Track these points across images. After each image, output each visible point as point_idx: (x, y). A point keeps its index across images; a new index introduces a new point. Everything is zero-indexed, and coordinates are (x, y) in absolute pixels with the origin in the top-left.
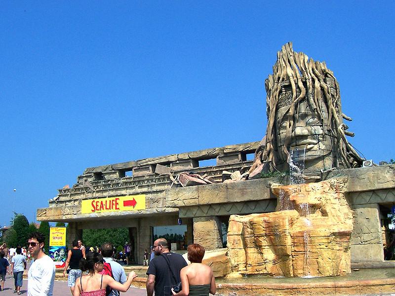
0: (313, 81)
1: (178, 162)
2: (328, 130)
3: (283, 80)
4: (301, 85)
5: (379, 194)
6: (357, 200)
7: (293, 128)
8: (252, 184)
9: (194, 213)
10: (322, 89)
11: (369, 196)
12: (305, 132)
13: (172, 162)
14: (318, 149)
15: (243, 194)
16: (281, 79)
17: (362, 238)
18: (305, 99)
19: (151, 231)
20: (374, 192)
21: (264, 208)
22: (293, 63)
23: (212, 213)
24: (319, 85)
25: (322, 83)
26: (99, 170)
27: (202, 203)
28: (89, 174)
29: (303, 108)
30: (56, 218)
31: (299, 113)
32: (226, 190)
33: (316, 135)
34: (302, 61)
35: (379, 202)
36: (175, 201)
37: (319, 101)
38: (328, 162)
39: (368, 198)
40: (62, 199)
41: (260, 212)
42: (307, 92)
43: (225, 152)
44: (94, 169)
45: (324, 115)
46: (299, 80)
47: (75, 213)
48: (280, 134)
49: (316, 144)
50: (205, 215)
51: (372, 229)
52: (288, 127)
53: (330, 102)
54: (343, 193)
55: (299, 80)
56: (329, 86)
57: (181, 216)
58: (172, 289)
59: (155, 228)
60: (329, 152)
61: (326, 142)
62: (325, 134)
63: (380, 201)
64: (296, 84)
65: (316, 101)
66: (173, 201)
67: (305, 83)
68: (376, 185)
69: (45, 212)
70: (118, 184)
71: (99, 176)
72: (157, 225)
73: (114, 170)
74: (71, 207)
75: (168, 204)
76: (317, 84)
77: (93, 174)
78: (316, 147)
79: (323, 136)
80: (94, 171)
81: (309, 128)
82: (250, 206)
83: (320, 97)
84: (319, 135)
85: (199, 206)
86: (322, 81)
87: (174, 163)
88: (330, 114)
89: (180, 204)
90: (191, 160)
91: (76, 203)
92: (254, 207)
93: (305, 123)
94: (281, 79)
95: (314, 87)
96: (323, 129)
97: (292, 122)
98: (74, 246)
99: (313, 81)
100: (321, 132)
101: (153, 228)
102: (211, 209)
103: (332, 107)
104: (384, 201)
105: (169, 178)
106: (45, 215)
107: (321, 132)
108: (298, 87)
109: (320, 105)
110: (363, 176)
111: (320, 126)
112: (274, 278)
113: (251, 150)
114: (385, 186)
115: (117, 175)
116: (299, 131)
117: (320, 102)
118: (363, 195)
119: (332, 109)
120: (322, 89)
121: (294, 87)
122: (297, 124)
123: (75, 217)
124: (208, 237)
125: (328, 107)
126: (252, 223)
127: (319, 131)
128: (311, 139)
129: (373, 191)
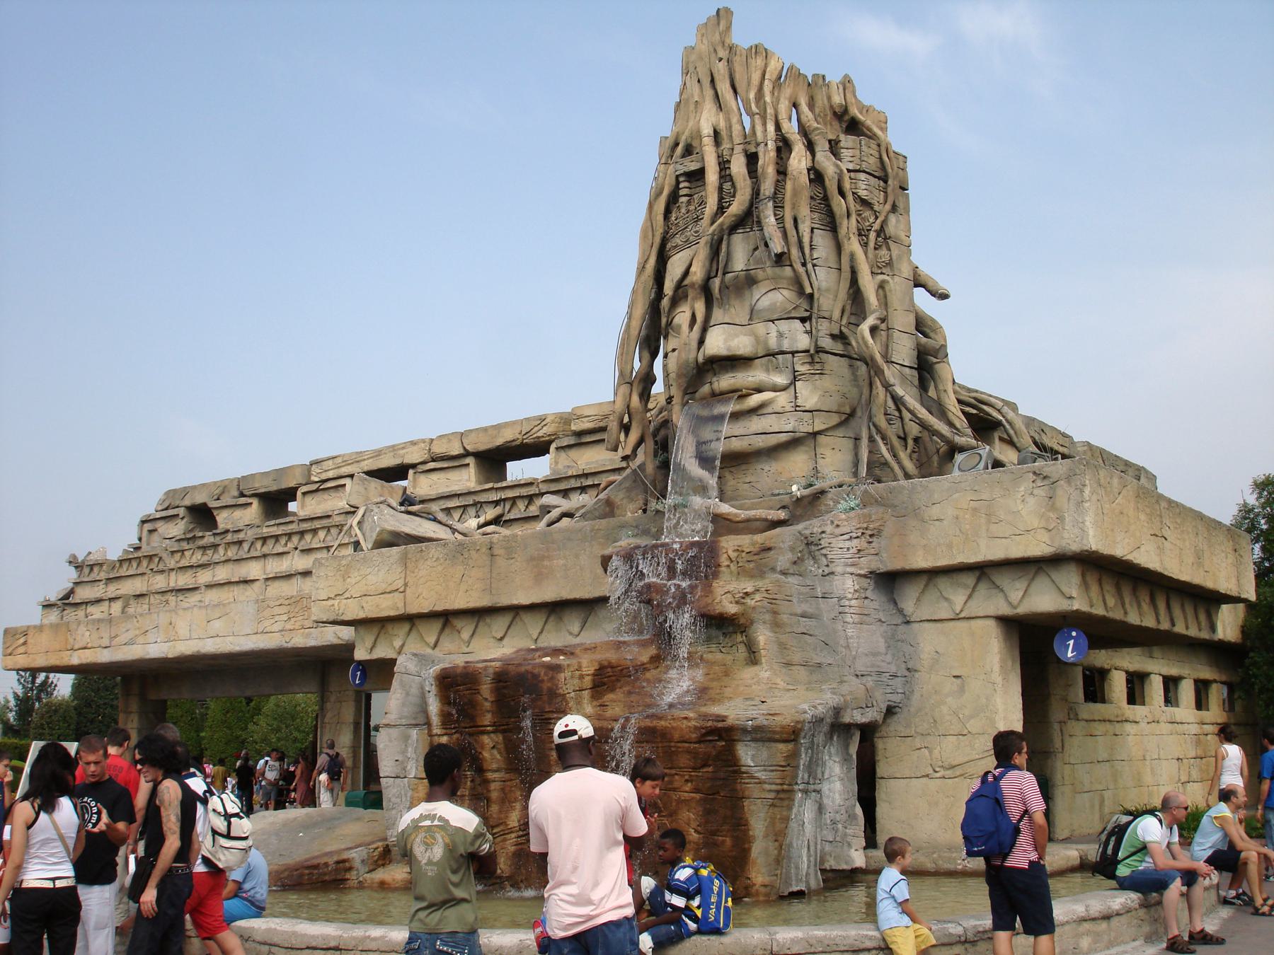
0: (784, 146)
1: (432, 465)
2: (833, 336)
4: (738, 166)
5: (998, 583)
6: (910, 598)
8: (569, 539)
9: (397, 643)
10: (817, 176)
11: (966, 586)
12: (741, 344)
13: (414, 466)
14: (789, 407)
16: (679, 150)
17: (936, 752)
18: (748, 219)
19: (358, 710)
20: (983, 571)
22: (724, 88)
25: (819, 156)
26: (199, 499)
27: (414, 609)
28: (170, 512)
29: (740, 255)
30: (76, 659)
32: (488, 563)
33: (783, 353)
34: (756, 77)
35: (1000, 613)
36: (336, 602)
37: (801, 227)
38: (833, 461)
39: (958, 598)
40: (83, 593)
42: (756, 193)
43: (573, 428)
44: (186, 491)
45: (824, 279)
47: (106, 642)
49: (784, 389)
51: (971, 717)
52: (685, 328)
53: (848, 227)
54: (773, 569)
56: (844, 167)
57: (360, 654)
58: (188, 917)
59: (374, 695)
60: (844, 417)
61: (826, 382)
62: (819, 350)
63: (1005, 610)
64: (724, 165)
65: (789, 224)
66: (330, 602)
68: (983, 543)
69: (22, 641)
70: (240, 543)
71: (202, 515)
72: (376, 690)
73: (243, 491)
74: (99, 620)
75: (317, 612)
76: (799, 161)
77: (181, 512)
78: (783, 400)
79: (815, 354)
80: (187, 502)
81: (760, 328)
83: (805, 212)
84: (793, 353)
85: (411, 620)
87: (421, 468)
88: (846, 274)
89: (353, 611)
91: (117, 607)
92: (576, 629)
93: (747, 311)
95: (782, 172)
96: (809, 333)
97: (700, 307)
99: (784, 146)
100: (803, 342)
101: (369, 698)
102: (447, 631)
103: (854, 245)
106: (22, 650)
109: (806, 240)
110: (935, 511)
111: (803, 320)
112: (509, 899)
114: (1017, 552)
115: (253, 512)
116: (717, 343)
117: (805, 228)
118: (943, 583)
119: (852, 257)
120: (817, 176)
121: (712, 176)
122: (717, 314)
123: (104, 657)
125: (839, 248)
127: (794, 340)
128: (767, 371)
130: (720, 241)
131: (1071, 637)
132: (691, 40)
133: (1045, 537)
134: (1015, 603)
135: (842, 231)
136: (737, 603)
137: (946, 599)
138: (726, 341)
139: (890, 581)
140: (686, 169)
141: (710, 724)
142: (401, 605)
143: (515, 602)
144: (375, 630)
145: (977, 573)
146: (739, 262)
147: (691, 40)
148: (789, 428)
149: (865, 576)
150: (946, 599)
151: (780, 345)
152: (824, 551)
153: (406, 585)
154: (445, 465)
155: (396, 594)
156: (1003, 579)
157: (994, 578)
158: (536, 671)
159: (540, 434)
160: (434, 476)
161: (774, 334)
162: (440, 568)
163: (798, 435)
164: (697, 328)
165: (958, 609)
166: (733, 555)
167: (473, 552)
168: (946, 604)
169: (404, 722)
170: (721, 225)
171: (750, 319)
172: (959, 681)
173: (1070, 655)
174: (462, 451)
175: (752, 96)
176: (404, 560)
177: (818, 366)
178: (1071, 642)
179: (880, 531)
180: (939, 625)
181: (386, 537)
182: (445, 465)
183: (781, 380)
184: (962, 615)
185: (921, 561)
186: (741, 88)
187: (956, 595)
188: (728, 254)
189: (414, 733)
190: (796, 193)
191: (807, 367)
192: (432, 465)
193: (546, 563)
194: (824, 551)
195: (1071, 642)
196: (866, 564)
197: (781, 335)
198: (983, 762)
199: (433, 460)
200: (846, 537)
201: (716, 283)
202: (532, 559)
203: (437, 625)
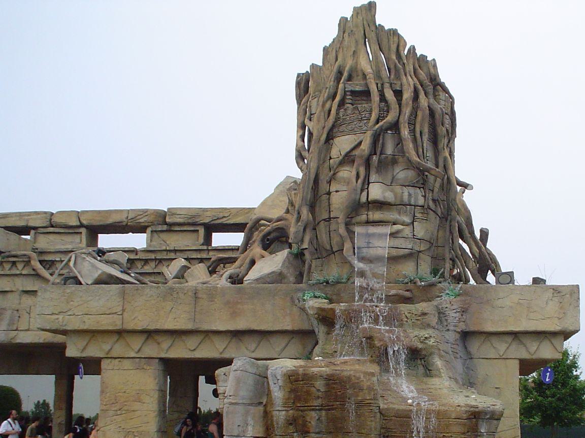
3: (350, 78)
4: (389, 95)
5: (553, 342)
7: (363, 183)
9: (106, 347)
13: (35, 228)
14: (410, 235)
15: (234, 314)
16: (345, 75)
21: (278, 349)
23: (151, 350)
24: (426, 105)
31: (381, 154)
33: (410, 205)
36: (61, 317)
37: (424, 137)
41: (291, 357)
46: (387, 85)
48: (329, 193)
50: (133, 355)
55: (387, 85)
65: (418, 135)
67: (398, 94)
82: (271, 341)
86: (431, 97)
90: (83, 230)
94: (345, 75)
96: (425, 197)
97: (362, 171)
98: (76, 425)
100: (421, 201)
102: (150, 341)
104: (534, 357)
105: (28, 263)
107: (421, 201)
108: (383, 98)
113: (226, 224)
116: (376, 191)
118: (495, 341)
121: (375, 97)
124: (137, 406)
126: (470, 383)
127: (416, 199)
128: (399, 213)
129: (515, 335)
130: (379, 135)
131: (548, 372)
132: (348, 14)
133: (556, 321)
134: (532, 352)
135: (440, 146)
136: (422, 342)
137: (494, 348)
138: (383, 193)
139: (466, 335)
140: (353, 89)
141: (472, 409)
142: (119, 323)
143: (214, 328)
144: (87, 338)
145: (513, 336)
146: (389, 150)
147: (348, 14)
148: (410, 246)
149: (459, 333)
150: (494, 348)
151: (409, 200)
152: (446, 318)
153: (123, 310)
154: (67, 231)
155: (115, 316)
156: (527, 340)
157: (520, 339)
158: (358, 375)
159: (140, 221)
160: (51, 237)
161: (406, 194)
162: (153, 302)
163: (413, 251)
164: (360, 181)
165: (501, 353)
166: (409, 315)
167: (181, 295)
168: (494, 350)
169: (245, 401)
170: (382, 126)
171: (391, 183)
172: (498, 390)
173: (547, 380)
174: (79, 224)
175: (394, 57)
176: (123, 294)
177: (425, 215)
178: (548, 374)
179: (467, 309)
180: (488, 360)
181: (104, 277)
182: (67, 231)
183: (407, 219)
184: (503, 357)
185: (490, 328)
186: (385, 48)
187: (501, 346)
188: (383, 144)
189: (252, 409)
190: (423, 119)
191: (421, 215)
192: (51, 230)
193: (239, 306)
194: (446, 318)
195: (548, 374)
196: (462, 327)
197: (410, 195)
198: (510, 431)
199: (52, 226)
200: (455, 311)
201: (375, 158)
202: (228, 303)
203: (142, 338)
